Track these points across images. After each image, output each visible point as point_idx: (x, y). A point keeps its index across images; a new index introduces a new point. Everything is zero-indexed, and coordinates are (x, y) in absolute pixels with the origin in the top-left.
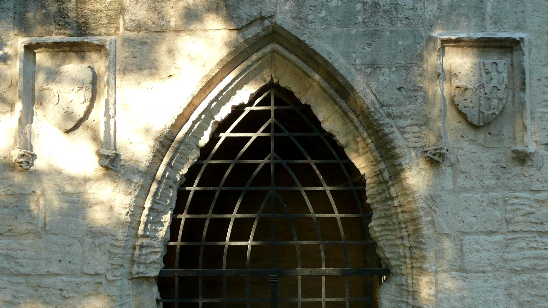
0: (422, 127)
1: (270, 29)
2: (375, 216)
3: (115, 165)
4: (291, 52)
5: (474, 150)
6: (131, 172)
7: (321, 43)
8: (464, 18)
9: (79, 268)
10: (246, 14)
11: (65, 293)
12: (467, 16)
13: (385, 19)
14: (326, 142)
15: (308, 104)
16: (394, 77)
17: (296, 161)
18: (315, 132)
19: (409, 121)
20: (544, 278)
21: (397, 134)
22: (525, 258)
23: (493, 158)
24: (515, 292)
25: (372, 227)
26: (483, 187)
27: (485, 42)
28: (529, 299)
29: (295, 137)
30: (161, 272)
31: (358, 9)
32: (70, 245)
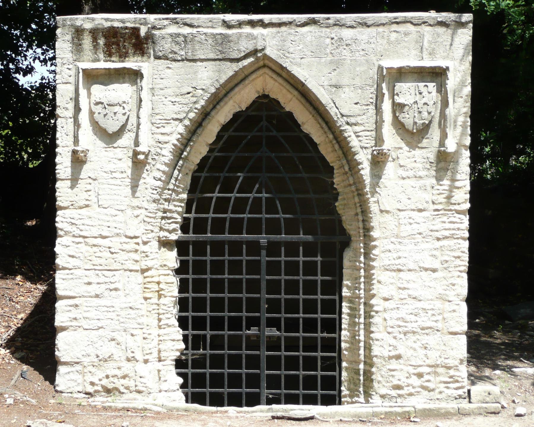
7: (299, 69)
16: (352, 95)
17: (281, 155)
19: (362, 128)
31: (327, 43)
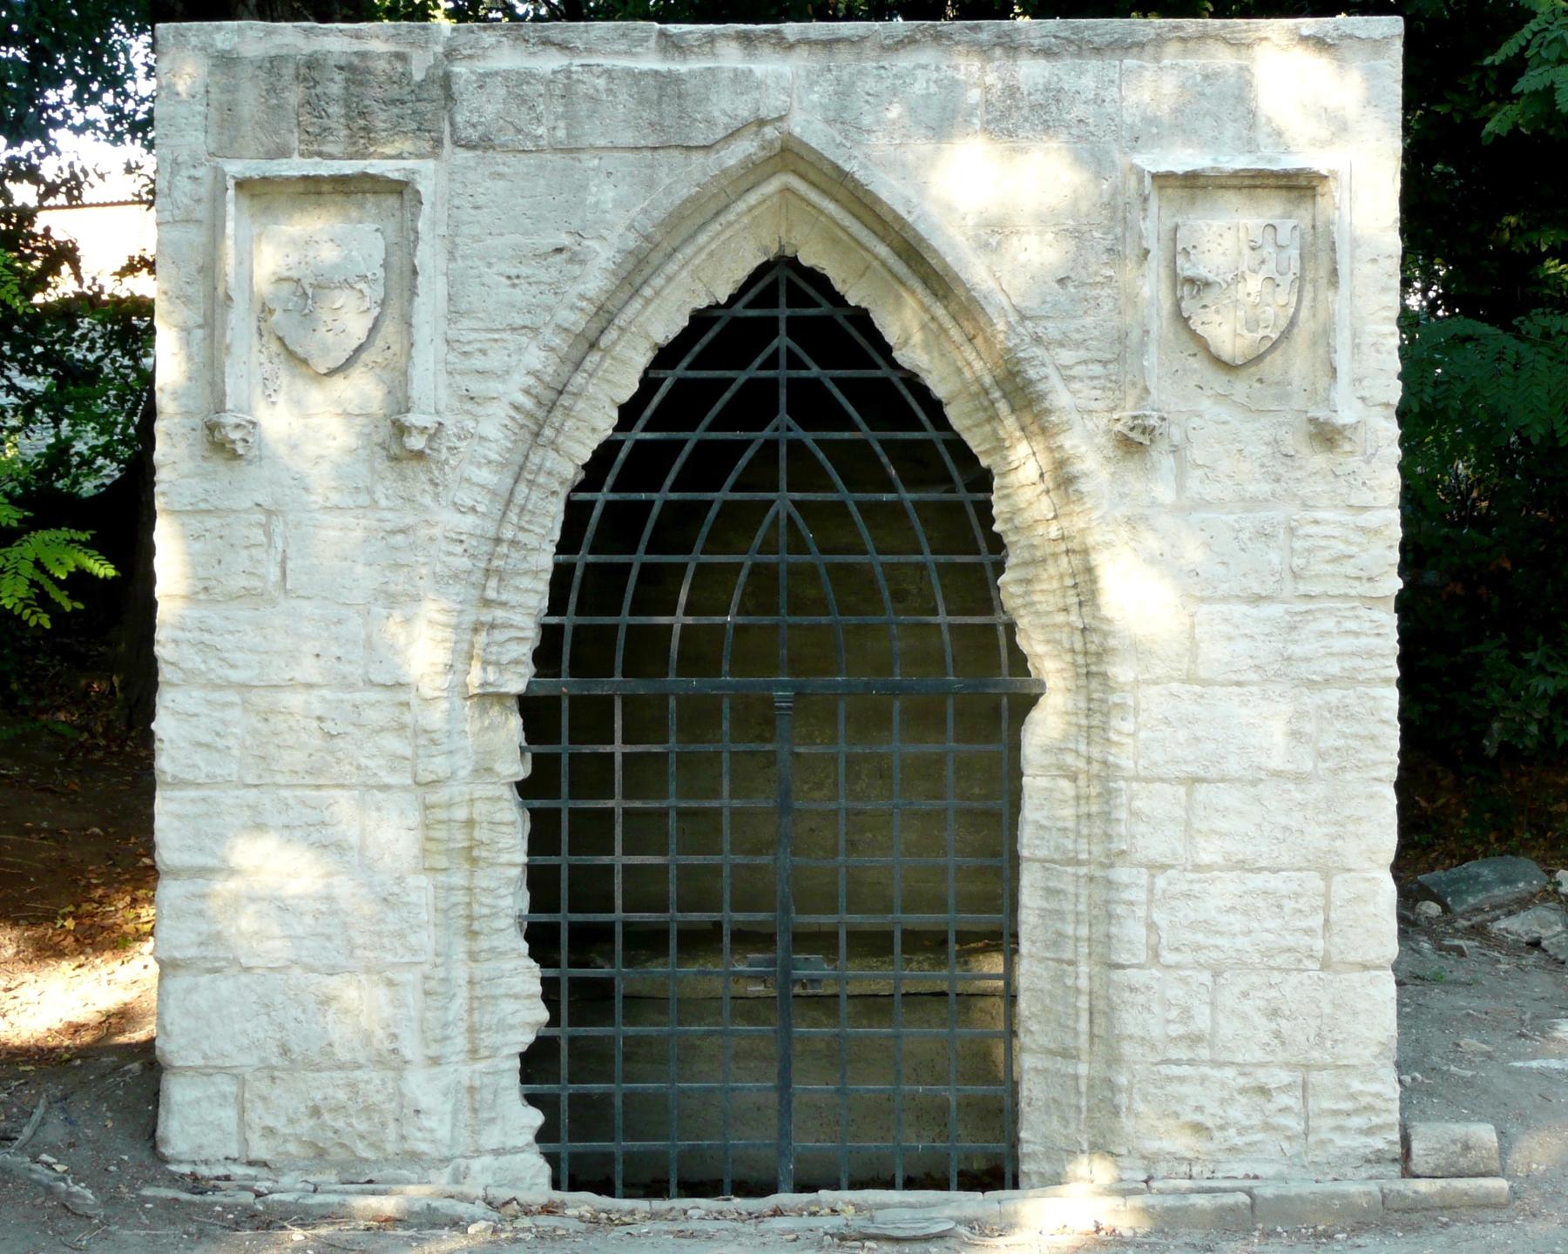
0: (1111, 366)
1: (777, 145)
2: (1011, 561)
3: (435, 446)
4: (825, 192)
5: (1225, 417)
6: (471, 463)
8: (1209, 121)
9: (360, 671)
10: (725, 113)
11: (329, 726)
12: (1217, 119)
13: (1032, 124)
14: (905, 391)
15: (863, 305)
18: (877, 367)
20: (1374, 698)
21: (1055, 380)
22: (1332, 654)
23: (1266, 435)
24: (1309, 727)
25: (1005, 584)
26: (1243, 499)
27: (1253, 177)
28: (1341, 743)
29: (833, 380)
30: (529, 683)
32: (339, 622)
